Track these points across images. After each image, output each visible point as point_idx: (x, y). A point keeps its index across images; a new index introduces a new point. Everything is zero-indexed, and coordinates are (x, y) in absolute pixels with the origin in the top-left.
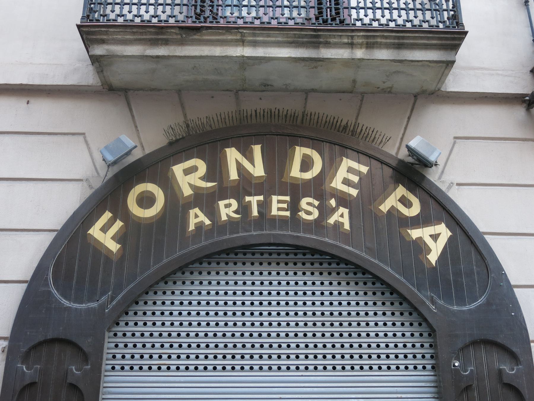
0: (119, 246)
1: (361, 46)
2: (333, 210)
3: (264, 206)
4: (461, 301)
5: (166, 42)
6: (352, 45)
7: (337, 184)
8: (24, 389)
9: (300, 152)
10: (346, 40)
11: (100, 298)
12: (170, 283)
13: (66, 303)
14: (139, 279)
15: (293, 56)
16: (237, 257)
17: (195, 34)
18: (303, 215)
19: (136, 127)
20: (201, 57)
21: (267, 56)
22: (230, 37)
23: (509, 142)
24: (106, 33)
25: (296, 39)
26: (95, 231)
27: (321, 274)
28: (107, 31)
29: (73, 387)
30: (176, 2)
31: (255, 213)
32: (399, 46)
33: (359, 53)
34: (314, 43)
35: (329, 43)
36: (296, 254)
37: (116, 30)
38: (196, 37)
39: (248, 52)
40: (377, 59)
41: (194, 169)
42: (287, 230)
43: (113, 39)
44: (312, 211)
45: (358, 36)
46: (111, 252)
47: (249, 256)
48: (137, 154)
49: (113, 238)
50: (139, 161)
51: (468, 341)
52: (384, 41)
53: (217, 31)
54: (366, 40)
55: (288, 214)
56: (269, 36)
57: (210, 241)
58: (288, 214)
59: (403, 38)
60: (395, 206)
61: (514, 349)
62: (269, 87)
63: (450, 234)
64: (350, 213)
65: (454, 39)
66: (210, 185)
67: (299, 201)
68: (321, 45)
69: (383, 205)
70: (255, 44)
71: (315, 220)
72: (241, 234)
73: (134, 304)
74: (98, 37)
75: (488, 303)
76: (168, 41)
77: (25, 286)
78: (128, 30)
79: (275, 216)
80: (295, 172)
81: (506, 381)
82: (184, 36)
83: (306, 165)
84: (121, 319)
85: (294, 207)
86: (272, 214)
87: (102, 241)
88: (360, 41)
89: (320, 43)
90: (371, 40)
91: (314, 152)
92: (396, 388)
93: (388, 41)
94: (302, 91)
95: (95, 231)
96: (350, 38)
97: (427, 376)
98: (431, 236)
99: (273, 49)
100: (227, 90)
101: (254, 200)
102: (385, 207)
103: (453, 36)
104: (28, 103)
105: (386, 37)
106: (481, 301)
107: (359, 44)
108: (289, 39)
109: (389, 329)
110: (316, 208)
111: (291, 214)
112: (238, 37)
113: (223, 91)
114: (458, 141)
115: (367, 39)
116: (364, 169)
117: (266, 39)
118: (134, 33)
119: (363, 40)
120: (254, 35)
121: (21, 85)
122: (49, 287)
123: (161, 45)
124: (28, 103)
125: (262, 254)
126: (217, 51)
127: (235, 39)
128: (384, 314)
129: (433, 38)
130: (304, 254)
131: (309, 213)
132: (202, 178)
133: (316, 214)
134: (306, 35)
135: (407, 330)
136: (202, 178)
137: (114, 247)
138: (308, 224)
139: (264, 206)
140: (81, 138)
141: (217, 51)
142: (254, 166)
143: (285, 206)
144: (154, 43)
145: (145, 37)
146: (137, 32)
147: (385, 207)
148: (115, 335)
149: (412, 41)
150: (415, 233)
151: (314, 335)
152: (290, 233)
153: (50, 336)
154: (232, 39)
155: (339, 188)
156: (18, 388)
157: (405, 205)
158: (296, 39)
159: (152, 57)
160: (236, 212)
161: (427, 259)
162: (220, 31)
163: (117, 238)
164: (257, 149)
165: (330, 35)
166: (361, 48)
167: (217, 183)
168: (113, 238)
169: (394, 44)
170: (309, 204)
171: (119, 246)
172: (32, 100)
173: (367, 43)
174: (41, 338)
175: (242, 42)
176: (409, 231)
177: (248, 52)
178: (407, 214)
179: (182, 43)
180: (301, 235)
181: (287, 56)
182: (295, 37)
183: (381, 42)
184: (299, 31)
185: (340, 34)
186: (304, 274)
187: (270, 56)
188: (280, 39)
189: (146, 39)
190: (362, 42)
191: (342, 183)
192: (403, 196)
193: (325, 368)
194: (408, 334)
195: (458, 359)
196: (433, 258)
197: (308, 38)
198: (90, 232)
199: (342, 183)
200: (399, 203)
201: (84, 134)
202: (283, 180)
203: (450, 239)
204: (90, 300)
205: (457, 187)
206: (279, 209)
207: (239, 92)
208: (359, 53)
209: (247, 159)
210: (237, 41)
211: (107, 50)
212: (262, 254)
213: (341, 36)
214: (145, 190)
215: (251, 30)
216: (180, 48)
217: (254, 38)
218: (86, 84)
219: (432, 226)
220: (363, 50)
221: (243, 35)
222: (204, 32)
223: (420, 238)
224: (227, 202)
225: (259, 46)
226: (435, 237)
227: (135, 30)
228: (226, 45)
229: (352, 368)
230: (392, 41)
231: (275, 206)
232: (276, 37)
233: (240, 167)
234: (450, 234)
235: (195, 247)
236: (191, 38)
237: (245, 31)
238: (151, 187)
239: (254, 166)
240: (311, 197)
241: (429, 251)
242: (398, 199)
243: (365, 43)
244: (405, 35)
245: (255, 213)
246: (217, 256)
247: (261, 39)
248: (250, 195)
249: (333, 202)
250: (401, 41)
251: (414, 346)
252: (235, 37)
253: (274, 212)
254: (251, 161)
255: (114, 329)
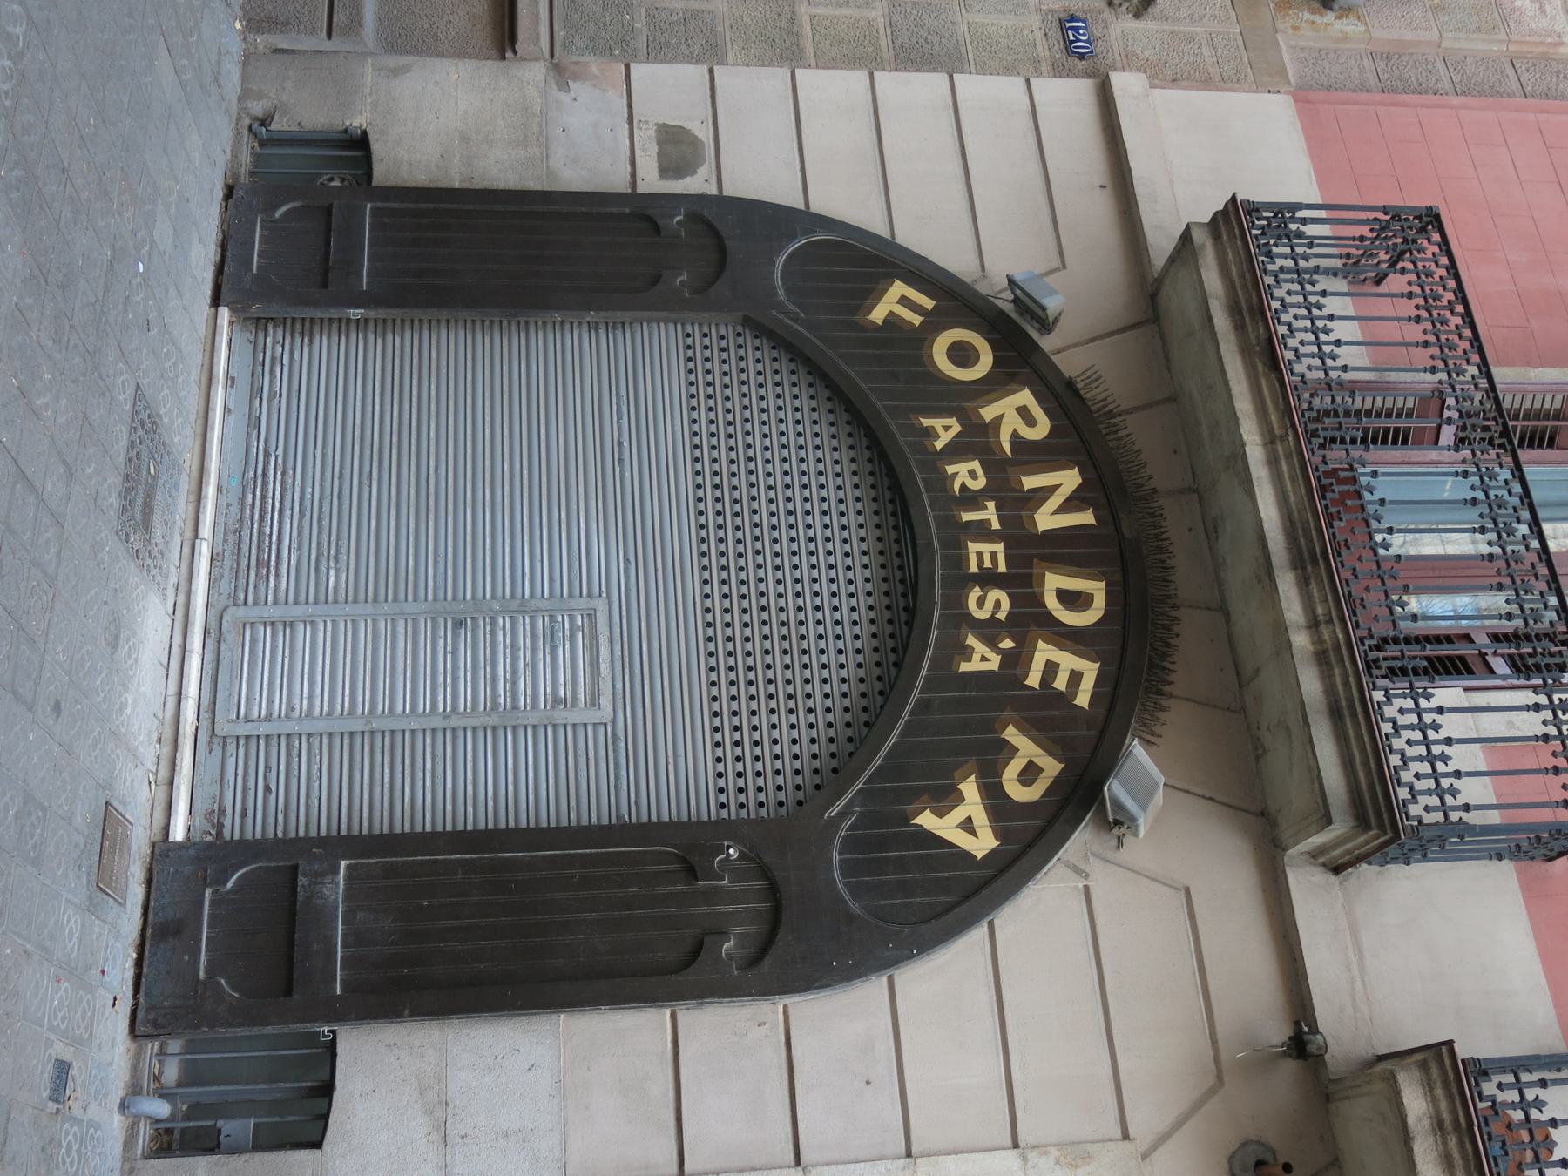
0: (880, 322)
1: (1318, 641)
2: (992, 643)
3: (981, 531)
4: (848, 869)
5: (1239, 327)
6: (1314, 625)
7: (1044, 652)
8: (650, 220)
9: (1097, 589)
10: (1320, 611)
11: (794, 303)
12: (829, 405)
13: (781, 260)
14: (830, 353)
15: (1266, 526)
16: (887, 503)
17: (1264, 364)
18: (975, 593)
19: (1093, 340)
20: (1226, 382)
21: (1255, 484)
22: (1274, 418)
23: (1202, 1004)
24: (1232, 237)
25: (1299, 525)
26: (898, 289)
27: (874, 636)
28: (1235, 236)
29: (657, 279)
30: (1564, 728)
31: (967, 517)
32: (1335, 713)
33: (1301, 640)
34: (1302, 560)
35: (1307, 584)
36: (902, 581)
37: (1241, 252)
38: (1260, 367)
39: (1255, 453)
40: (1297, 677)
41: (1029, 420)
42: (943, 567)
43: (1224, 251)
44: (984, 609)
45: (1335, 631)
46: (869, 313)
47: (891, 521)
48: (1047, 343)
49: (891, 313)
50: (1036, 347)
51: (775, 873)
52: (1338, 680)
53: (1280, 395)
54: (1330, 647)
55: (974, 568)
56: (1293, 479)
57: (906, 450)
58: (974, 568)
59: (1354, 715)
60: (1018, 754)
61: (767, 961)
62: (1214, 535)
63: (979, 855)
64: (990, 673)
65: (1378, 814)
66: (1007, 447)
67: (1002, 588)
68: (1300, 572)
69: (1016, 731)
70: (1272, 461)
71: (969, 614)
72: (925, 495)
73: (790, 356)
74: (1223, 229)
75: (851, 918)
76: (1243, 328)
77: (802, 207)
78: (1245, 266)
79: (967, 548)
80: (1054, 582)
81: (707, 940)
82: (1258, 349)
83: (1071, 599)
84: (765, 341)
85: (988, 579)
86: (970, 544)
87: (884, 299)
88: (1326, 637)
89: (1304, 568)
90: (1332, 658)
91: (1100, 614)
92: (683, 755)
93: (1340, 688)
94: (1223, 600)
95: (898, 289)
96: (1328, 617)
97: (706, 808)
98: (969, 819)
99: (1272, 492)
100: (1194, 474)
101: (990, 514)
102: (1011, 734)
103: (1383, 810)
104: (1102, 187)
105: (1346, 683)
106: (854, 906)
107: (1319, 638)
108: (1296, 514)
109: (787, 750)
110: (993, 615)
111: (974, 574)
112: (1277, 432)
113: (1192, 468)
114: (1182, 895)
115: (1334, 650)
116: (1083, 699)
117: (1286, 476)
118: (1242, 276)
119: (1328, 642)
120: (1288, 456)
121: (1130, 170)
122: (802, 236)
123: (1232, 321)
124: (1102, 187)
125: (897, 541)
126: (1244, 404)
127: (1272, 428)
128: (813, 741)
129: (1368, 773)
130: (904, 595)
131: (981, 603)
132: (1015, 434)
133: (982, 615)
134: (1312, 540)
135: (788, 780)
136: (1015, 434)
137: (878, 314)
138: (961, 602)
139: (981, 531)
140: (1056, 263)
141: (1244, 404)
142: (1053, 514)
143: (988, 564)
144: (1234, 310)
145: (1240, 292)
146: (1245, 279)
147: (1011, 734)
148: (739, 335)
149: (1351, 732)
150: (969, 788)
151: (773, 711)
152: (939, 572)
153: (727, 243)
154: (1271, 423)
155: (1037, 654)
156: (650, 212)
157: (1023, 773)
158: (1299, 525)
159: (1208, 310)
160: (963, 487)
161: (924, 810)
162: (1281, 400)
163: (892, 320)
164: (1086, 518)
165: (1323, 581)
166: (1313, 643)
167: (1010, 455)
168: (891, 313)
169: (1337, 701)
170: (998, 604)
171: (880, 322)
172: (1108, 192)
173: (1325, 652)
174: (724, 232)
175: (1270, 441)
176: (973, 778)
177: (1255, 453)
178: (1005, 776)
179: (1245, 350)
180: (939, 591)
181: (1263, 515)
182: (1302, 524)
183: (1334, 675)
184: (1315, 525)
185: (1330, 598)
186: (869, 594)
187: (1256, 489)
188: (1292, 499)
189: (1237, 296)
190: (1325, 642)
191: (1048, 660)
192: (1041, 770)
193: (716, 729)
194: (780, 780)
195: (742, 856)
196: (927, 820)
197: (1307, 545)
198: (897, 283)
199: (1048, 660)
200: (1024, 762)
201: (1064, 267)
202: (1035, 560)
203: (968, 856)
204: (788, 291)
205: (1081, 885)
206: (980, 555)
207: (1196, 495)
208: (1301, 640)
209: (1065, 501)
210: (1271, 431)
211: (1204, 245)
212: (897, 541)
213: (1327, 600)
214: (980, 352)
215: (1296, 449)
216: (1235, 348)
217: (1282, 457)
218: (1151, 257)
219: (990, 822)
220: (1310, 648)
221: (1284, 438)
222: (1273, 376)
223: (960, 799)
224: (980, 472)
225: (1270, 469)
226: (968, 826)
227: (1247, 275)
228: (1258, 417)
229: (714, 699)
230: (1342, 695)
231: (986, 548)
232: (1295, 493)
233: (1048, 492)
234: (979, 855)
235: (894, 428)
236: (1257, 360)
237: (1290, 439)
238: (986, 362)
239: (1053, 514)
240: (1011, 607)
241: (940, 814)
242: (1033, 760)
243: (1325, 645)
244: (1360, 717)
245: (967, 517)
246: (884, 472)
247: (1285, 468)
248: (998, 509)
249: (1007, 644)
250: (1346, 712)
251: (760, 789)
252: (1275, 426)
253: (973, 547)
254: (1064, 508)
255: (747, 332)
